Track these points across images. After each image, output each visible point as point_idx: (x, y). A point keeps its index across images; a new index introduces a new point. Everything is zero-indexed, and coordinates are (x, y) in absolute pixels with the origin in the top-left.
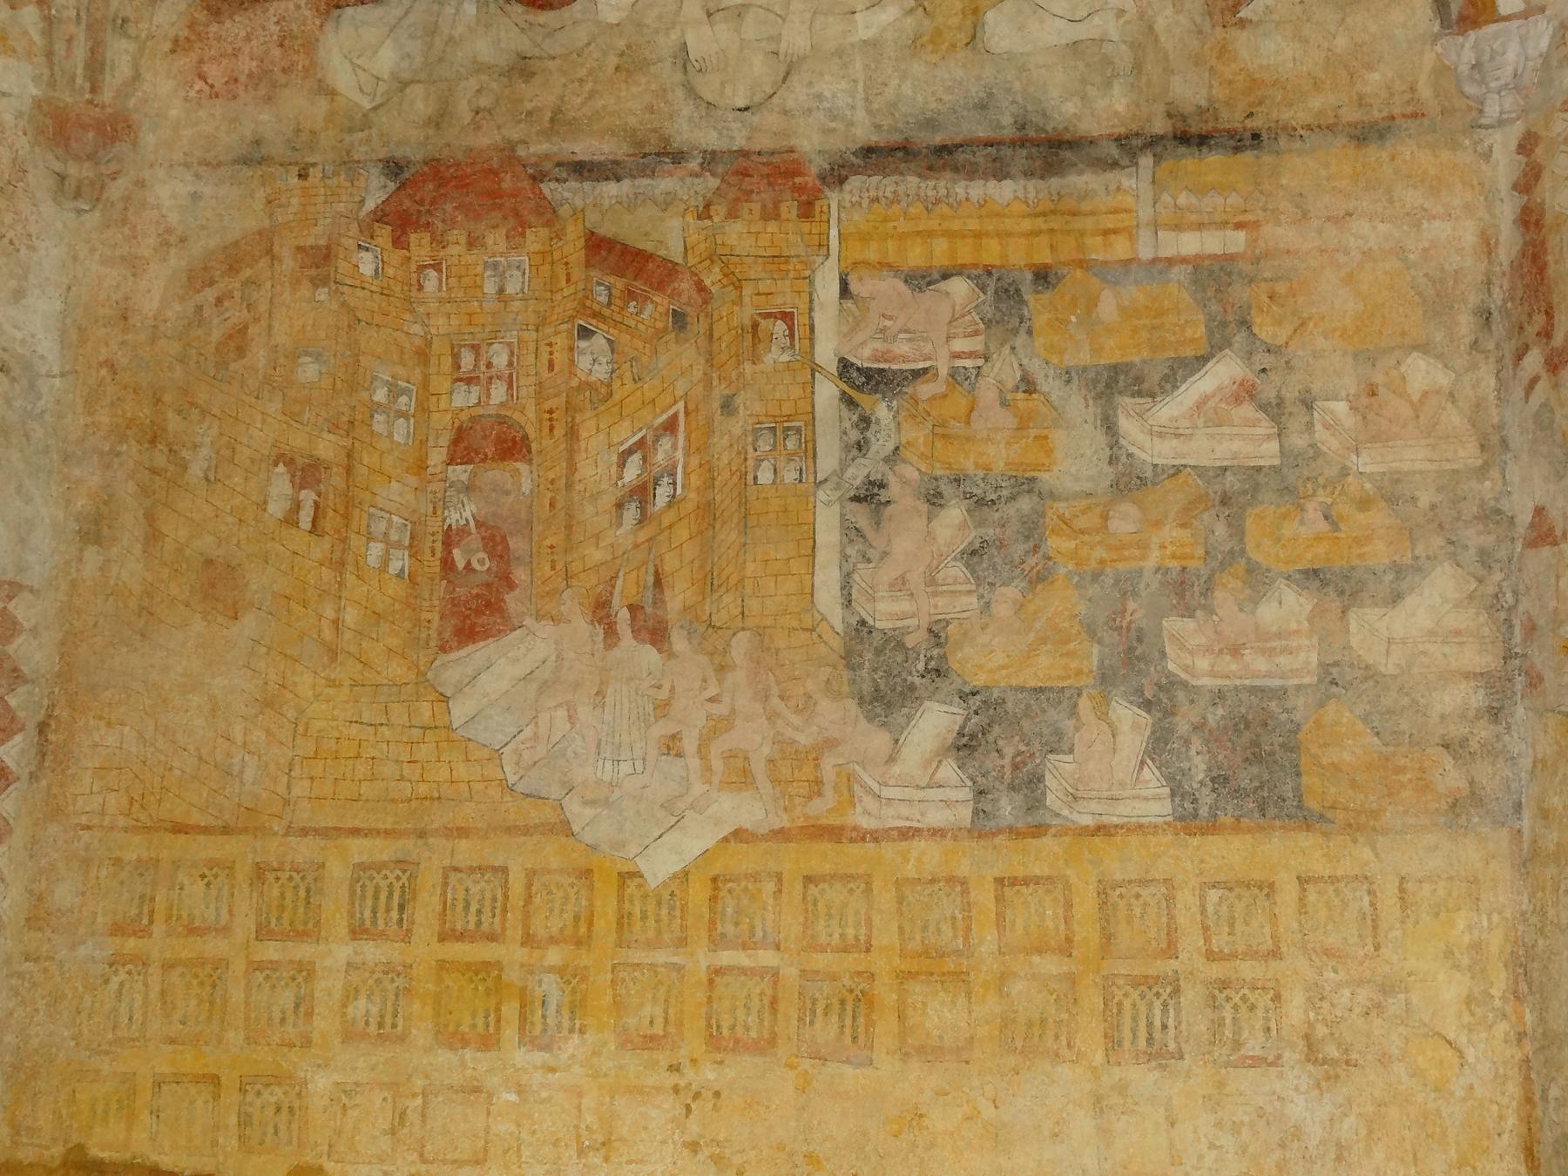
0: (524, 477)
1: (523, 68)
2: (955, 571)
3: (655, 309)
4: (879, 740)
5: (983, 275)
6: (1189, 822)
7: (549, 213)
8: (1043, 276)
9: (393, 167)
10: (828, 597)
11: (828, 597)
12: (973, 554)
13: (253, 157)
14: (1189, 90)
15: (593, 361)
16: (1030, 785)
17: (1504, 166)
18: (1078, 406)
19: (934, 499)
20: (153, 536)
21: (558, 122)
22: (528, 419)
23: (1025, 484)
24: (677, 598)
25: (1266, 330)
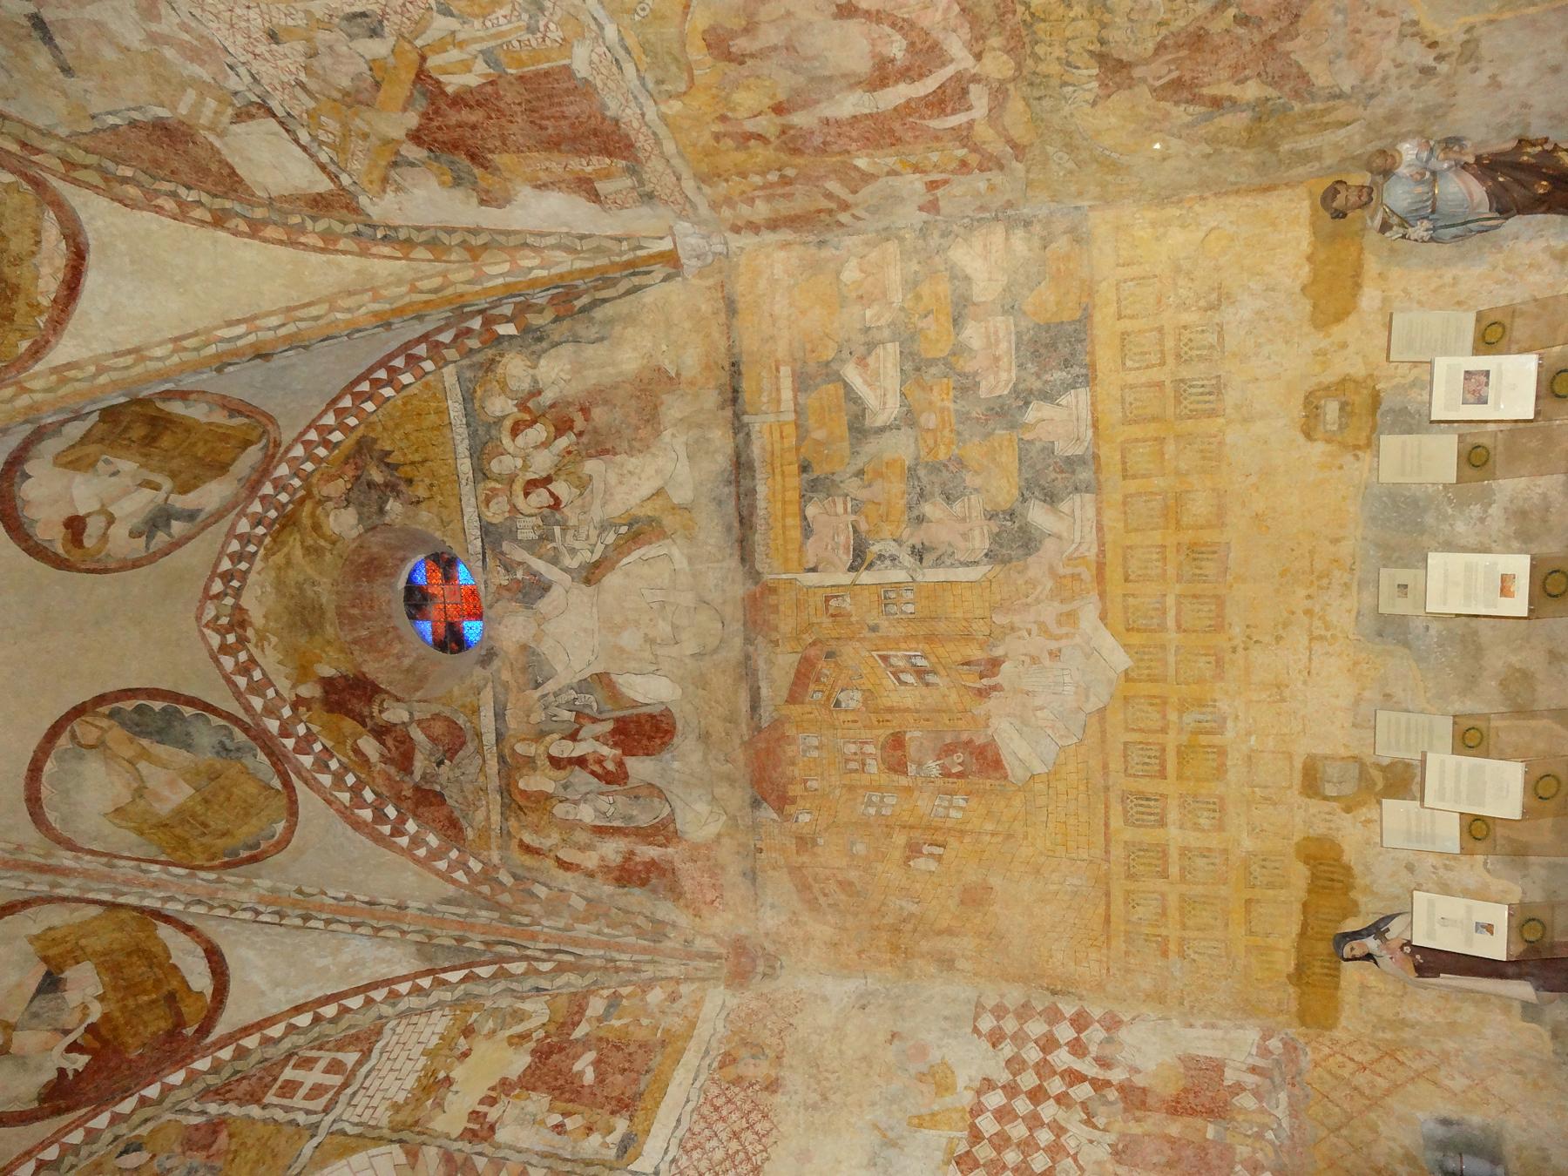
0: (913, 735)
1: (704, 737)
2: (957, 507)
3: (825, 667)
4: (1049, 545)
5: (804, 499)
6: (1089, 379)
7: (777, 724)
8: (804, 468)
9: (756, 804)
10: (974, 574)
11: (974, 574)
12: (948, 498)
13: (752, 876)
14: (711, 399)
15: (852, 700)
16: (1071, 463)
17: (747, 240)
18: (871, 447)
19: (920, 519)
20: (949, 932)
21: (731, 719)
22: (883, 733)
23: (912, 472)
24: (975, 653)
25: (830, 354)
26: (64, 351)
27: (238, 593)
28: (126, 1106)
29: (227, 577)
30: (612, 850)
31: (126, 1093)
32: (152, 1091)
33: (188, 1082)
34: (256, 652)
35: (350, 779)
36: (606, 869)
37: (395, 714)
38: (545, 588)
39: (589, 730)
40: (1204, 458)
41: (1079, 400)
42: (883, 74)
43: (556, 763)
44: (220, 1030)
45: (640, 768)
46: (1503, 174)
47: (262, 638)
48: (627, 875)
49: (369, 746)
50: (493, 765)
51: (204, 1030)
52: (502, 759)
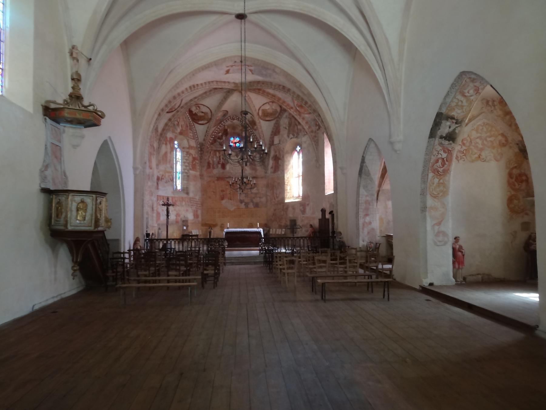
1: (223, 173)
16: (247, 206)
26: (261, 121)
27: (236, 120)
28: (189, 116)
29: (238, 119)
30: (211, 162)
31: (190, 116)
32: (190, 118)
33: (190, 121)
34: (230, 121)
35: (217, 132)
36: (209, 161)
37: (224, 138)
38: (237, 157)
39: (223, 160)
40: (158, 179)
41: (252, 207)
42: (276, 194)
43: (220, 157)
44: (194, 123)
45: (220, 166)
46: (373, 258)
47: (232, 122)
48: (209, 164)
49: (220, 134)
50: (219, 149)
51: (195, 122)
52: (220, 150)
